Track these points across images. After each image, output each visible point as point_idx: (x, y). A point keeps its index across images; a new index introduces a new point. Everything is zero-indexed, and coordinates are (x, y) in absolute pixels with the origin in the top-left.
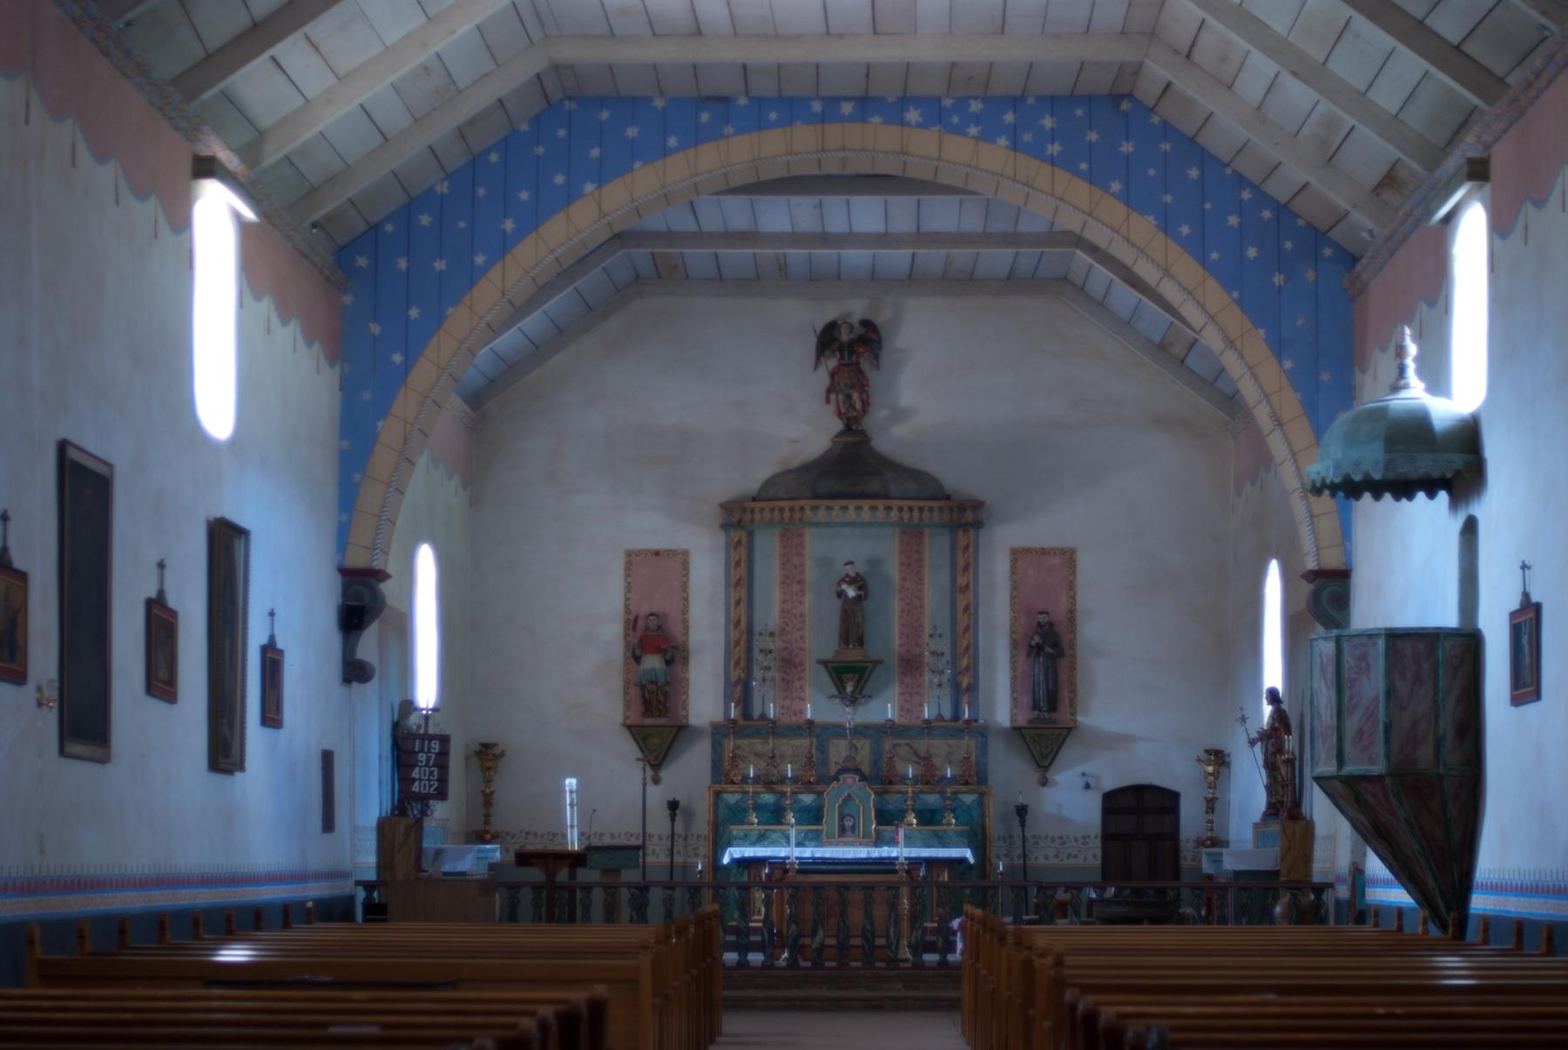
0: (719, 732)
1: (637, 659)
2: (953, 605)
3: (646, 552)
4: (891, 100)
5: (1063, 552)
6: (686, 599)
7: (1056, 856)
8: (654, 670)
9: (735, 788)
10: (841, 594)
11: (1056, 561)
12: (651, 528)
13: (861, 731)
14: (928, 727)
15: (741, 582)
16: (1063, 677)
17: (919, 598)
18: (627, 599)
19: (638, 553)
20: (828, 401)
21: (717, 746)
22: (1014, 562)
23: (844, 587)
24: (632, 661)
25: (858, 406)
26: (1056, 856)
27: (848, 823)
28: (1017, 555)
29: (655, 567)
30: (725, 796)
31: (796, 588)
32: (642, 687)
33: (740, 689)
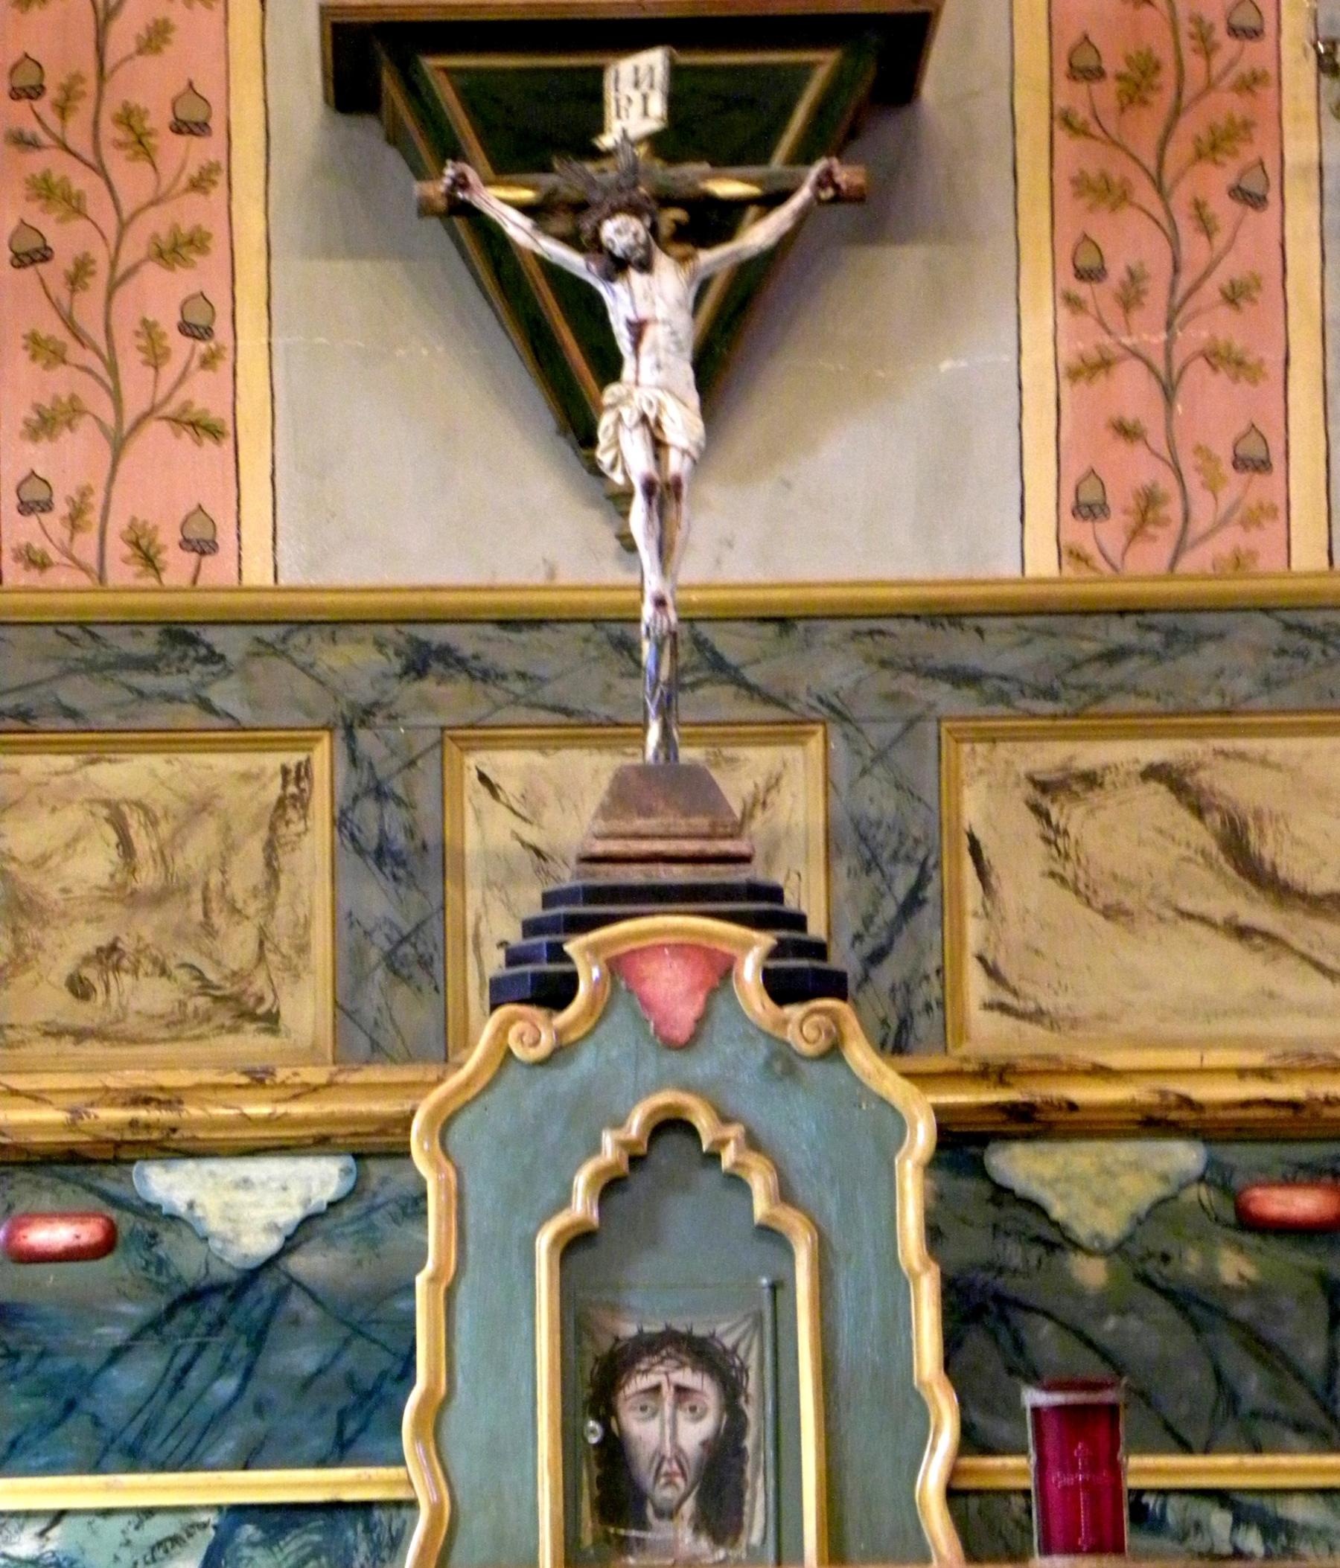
13: (741, 658)
27: (668, 1426)
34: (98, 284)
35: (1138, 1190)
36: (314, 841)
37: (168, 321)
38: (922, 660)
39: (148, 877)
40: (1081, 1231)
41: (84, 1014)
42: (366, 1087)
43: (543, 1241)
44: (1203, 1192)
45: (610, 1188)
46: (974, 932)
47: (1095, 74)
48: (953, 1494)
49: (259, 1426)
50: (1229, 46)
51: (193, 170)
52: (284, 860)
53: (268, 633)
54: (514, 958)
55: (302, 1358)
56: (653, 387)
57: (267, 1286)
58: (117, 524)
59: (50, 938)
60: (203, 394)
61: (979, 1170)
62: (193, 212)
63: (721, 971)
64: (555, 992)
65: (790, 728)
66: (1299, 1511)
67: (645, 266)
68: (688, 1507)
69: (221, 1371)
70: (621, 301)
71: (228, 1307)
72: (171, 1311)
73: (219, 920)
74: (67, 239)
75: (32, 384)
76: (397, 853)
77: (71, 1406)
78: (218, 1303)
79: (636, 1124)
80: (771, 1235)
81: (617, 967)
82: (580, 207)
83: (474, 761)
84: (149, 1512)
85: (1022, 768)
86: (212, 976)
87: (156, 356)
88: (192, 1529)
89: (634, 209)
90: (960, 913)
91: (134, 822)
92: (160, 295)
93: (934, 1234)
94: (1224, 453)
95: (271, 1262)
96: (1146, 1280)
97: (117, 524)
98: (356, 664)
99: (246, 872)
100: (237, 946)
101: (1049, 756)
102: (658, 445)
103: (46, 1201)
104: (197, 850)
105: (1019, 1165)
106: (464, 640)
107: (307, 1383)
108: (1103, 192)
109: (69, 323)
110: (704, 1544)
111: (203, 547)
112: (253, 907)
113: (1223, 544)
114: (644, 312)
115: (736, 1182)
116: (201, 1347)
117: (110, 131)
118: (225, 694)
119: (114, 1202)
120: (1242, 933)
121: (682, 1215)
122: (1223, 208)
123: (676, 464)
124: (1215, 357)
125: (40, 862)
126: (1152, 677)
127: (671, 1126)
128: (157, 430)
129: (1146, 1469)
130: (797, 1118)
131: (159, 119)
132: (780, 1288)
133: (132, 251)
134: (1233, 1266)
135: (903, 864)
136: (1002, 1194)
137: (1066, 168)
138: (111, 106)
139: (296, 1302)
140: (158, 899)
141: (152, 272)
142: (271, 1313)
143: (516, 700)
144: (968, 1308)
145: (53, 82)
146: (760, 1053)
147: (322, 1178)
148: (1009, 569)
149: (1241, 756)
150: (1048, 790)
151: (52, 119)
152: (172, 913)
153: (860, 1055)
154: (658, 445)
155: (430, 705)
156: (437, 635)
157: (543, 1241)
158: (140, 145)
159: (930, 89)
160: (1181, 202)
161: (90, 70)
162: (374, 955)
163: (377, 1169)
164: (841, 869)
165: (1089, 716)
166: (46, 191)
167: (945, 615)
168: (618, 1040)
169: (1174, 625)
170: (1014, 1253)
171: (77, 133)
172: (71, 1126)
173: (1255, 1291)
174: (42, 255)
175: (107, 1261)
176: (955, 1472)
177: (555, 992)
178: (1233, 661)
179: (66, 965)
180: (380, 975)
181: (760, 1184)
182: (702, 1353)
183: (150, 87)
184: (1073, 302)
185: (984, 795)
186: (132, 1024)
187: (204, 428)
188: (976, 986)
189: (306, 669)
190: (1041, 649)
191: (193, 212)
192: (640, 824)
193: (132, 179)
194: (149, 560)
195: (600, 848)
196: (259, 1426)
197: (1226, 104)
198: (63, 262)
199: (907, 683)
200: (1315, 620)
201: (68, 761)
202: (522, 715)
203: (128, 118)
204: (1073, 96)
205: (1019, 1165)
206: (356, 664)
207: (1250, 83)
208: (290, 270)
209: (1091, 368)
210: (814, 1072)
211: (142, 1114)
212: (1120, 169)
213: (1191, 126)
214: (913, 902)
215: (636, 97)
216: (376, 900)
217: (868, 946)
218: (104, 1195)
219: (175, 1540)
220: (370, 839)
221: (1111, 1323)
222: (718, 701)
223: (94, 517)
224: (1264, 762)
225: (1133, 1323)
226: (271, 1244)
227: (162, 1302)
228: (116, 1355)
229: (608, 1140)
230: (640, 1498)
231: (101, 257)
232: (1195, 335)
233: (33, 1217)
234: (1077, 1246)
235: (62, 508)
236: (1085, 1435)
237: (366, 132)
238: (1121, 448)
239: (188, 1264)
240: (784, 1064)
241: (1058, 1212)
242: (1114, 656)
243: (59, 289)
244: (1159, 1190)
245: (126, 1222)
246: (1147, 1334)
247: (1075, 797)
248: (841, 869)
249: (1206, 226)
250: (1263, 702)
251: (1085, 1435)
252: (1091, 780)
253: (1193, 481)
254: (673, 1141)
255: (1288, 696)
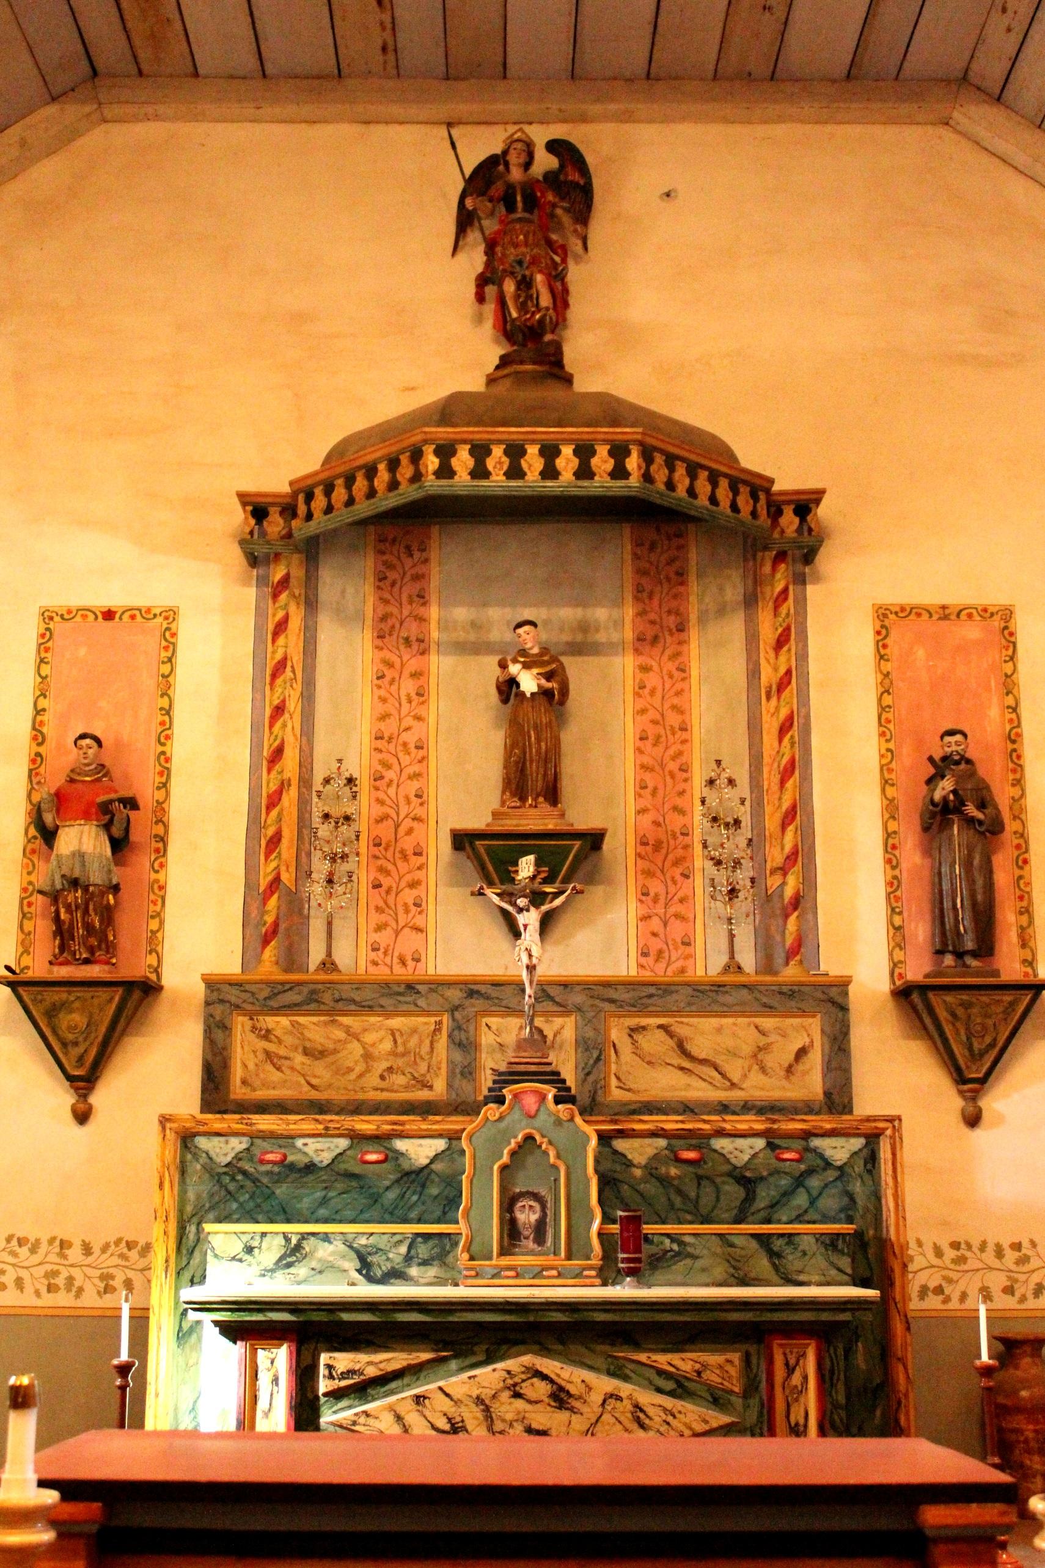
0: (222, 999)
1: (48, 835)
2: (754, 727)
3: (85, 611)
4: (528, 695)
5: (985, 612)
6: (168, 712)
7: (1009, 1290)
8: (80, 856)
9: (231, 1121)
10: (508, 688)
11: (972, 632)
12: (106, 569)
13: (555, 994)
14: (710, 996)
15: (282, 681)
16: (1002, 878)
17: (678, 710)
18: (38, 712)
19: (68, 615)
20: (480, 298)
21: (216, 1036)
22: (882, 635)
23: (514, 669)
24: (39, 842)
25: (545, 300)
26: (1009, 1290)
27: (527, 1216)
28: (887, 619)
29: (100, 642)
30: (202, 1142)
31: (408, 686)
32: (54, 897)
33: (276, 914)
34: (398, 586)
35: (651, 1152)
36: (443, 1040)
37: (410, 902)
38: (598, 997)
39: (400, 1049)
40: (635, 1162)
41: (383, 1085)
42: (451, 1121)
43: (496, 1167)
44: (667, 1152)
45: (513, 1154)
46: (613, 1067)
47: (647, 844)
48: (599, 1234)
49: (424, 1208)
50: (681, 838)
51: (418, 865)
52: (435, 1045)
53: (432, 986)
54: (490, 1090)
55: (434, 1191)
56: (530, 937)
57: (426, 1172)
58: (396, 954)
59: (375, 1065)
60: (419, 921)
61: (610, 1146)
62: (419, 875)
63: (543, 1098)
64: (501, 1101)
65: (566, 1013)
66: (687, 1239)
67: (528, 910)
68: (532, 1237)
69: (414, 1193)
70: (521, 919)
71: (415, 1177)
72: (402, 1177)
73: (418, 1060)
74: (386, 882)
75: (376, 918)
76: (465, 1043)
77: (376, 1201)
78: (413, 1176)
79: (520, 1137)
80: (555, 1167)
81: (516, 1096)
82: (511, 894)
83: (485, 1020)
84: (395, 1234)
85: (626, 1024)
86: (416, 1075)
87: (407, 911)
88: (405, 1238)
89: (525, 896)
90: (610, 1063)
91: (397, 1034)
92: (408, 896)
93: (597, 1161)
94: (679, 940)
95: (427, 1166)
96: (651, 1174)
97: (396, 954)
98: (455, 995)
99: (425, 1048)
100: (423, 1067)
101: (633, 1022)
102: (530, 956)
103: (371, 1149)
104: (413, 1042)
105: (620, 1144)
106: (483, 989)
107: (436, 1197)
108: (648, 874)
109: (386, 902)
110: (536, 1246)
111: (418, 960)
112: (427, 1057)
113: (679, 964)
114: (527, 922)
115: (546, 1153)
116: (409, 1188)
117: (398, 855)
118: (422, 1002)
119: (388, 1149)
120: (682, 1069)
121: (530, 1160)
122: (678, 877)
123: (535, 961)
124: (676, 916)
125: (373, 1045)
126: (660, 1002)
127: (529, 1138)
128: (407, 930)
129: (647, 1229)
130: (560, 1136)
131: (410, 852)
132: (556, 1180)
133: (403, 884)
134: (673, 1171)
135: (596, 1055)
136: (616, 1152)
137: (639, 867)
138: (398, 849)
139: (433, 1176)
140: (403, 1055)
141: (407, 890)
142: (427, 1179)
143: (495, 1005)
144: (607, 1182)
145: (386, 736)
146: (553, 1119)
147: (440, 1144)
148: (625, 973)
149: (682, 1023)
150: (633, 1031)
151: (383, 852)
152: (405, 1059)
153: (578, 1120)
154: (530, 956)
155: (473, 1006)
156: (475, 987)
157: (496, 1167)
158: (405, 857)
159: (605, 847)
160: (668, 875)
161: (393, 840)
162: (458, 1071)
163: (454, 1143)
164: (579, 1050)
165: (644, 1011)
166: (381, 869)
167: (607, 984)
168: (517, 1114)
169: (665, 989)
170: (618, 1168)
171: (389, 855)
172: (377, 1130)
173: (679, 1177)
174: (380, 886)
175: (384, 1165)
176: (600, 1229)
177: (501, 1101)
178: (681, 997)
179: (380, 1072)
180: (459, 1076)
181: (552, 1154)
182: (536, 1197)
183: (408, 844)
184: (641, 901)
185: (617, 1033)
186: (395, 1087)
187: (419, 930)
188: (614, 1082)
189: (442, 996)
190: (631, 994)
191: (419, 875)
192: (523, 1054)
193: (402, 866)
194: (403, 963)
195: (513, 1060)
196: (424, 1208)
197: (680, 852)
198: (386, 780)
199: (597, 1002)
200: (700, 988)
201: (381, 1019)
202: (498, 1009)
203: (402, 852)
204: (641, 849)
205: (620, 1144)
206: (455, 995)
207: (686, 847)
208: (442, 890)
209: (645, 918)
210: (566, 1124)
211: (395, 1127)
212: (653, 868)
213: (671, 857)
214: (598, 1059)
215: (526, 867)
216: (458, 1056)
217: (587, 1070)
218: (386, 1148)
219: (401, 1241)
220: (457, 1041)
221: (642, 1186)
222: (549, 1006)
223: (390, 952)
224: (687, 1024)
225: (648, 1186)
226: (427, 1161)
227: (399, 1175)
228: (387, 1188)
229: (513, 1141)
230: (520, 1233)
231: (394, 886)
232: (672, 910)
233: (367, 1152)
234: (634, 1166)
235: (382, 950)
236: (632, 1223)
237: (462, 856)
238: (654, 939)
239: (406, 1166)
240: (559, 1122)
241: (630, 1157)
242: (651, 996)
243: (384, 894)
244: (655, 1151)
245: (391, 1154)
246: (651, 1188)
247: (640, 1033)
248: (579, 1050)
249: (674, 882)
250: (688, 1009)
251: (632, 1223)
252: (644, 1028)
253: (671, 947)
254: (530, 1141)
255: (694, 1008)
